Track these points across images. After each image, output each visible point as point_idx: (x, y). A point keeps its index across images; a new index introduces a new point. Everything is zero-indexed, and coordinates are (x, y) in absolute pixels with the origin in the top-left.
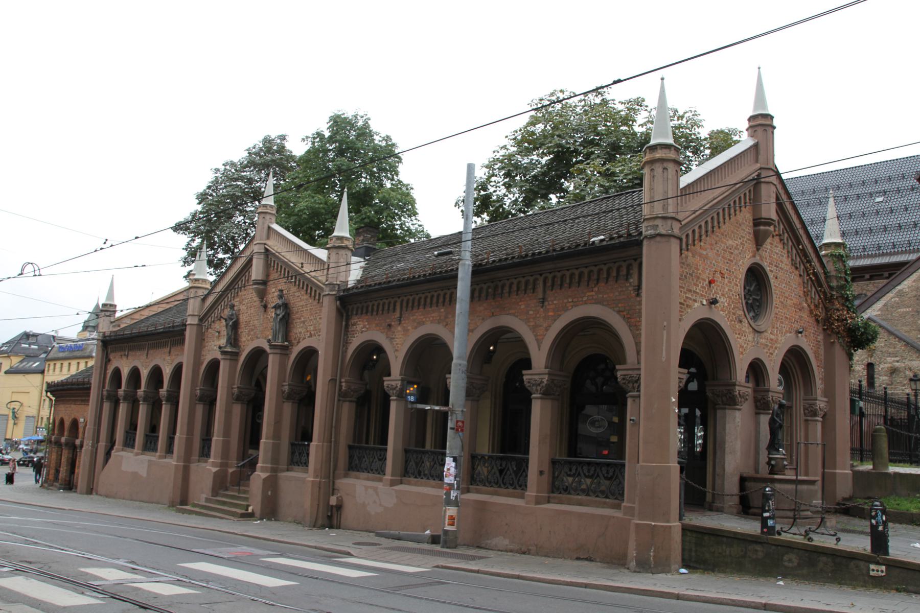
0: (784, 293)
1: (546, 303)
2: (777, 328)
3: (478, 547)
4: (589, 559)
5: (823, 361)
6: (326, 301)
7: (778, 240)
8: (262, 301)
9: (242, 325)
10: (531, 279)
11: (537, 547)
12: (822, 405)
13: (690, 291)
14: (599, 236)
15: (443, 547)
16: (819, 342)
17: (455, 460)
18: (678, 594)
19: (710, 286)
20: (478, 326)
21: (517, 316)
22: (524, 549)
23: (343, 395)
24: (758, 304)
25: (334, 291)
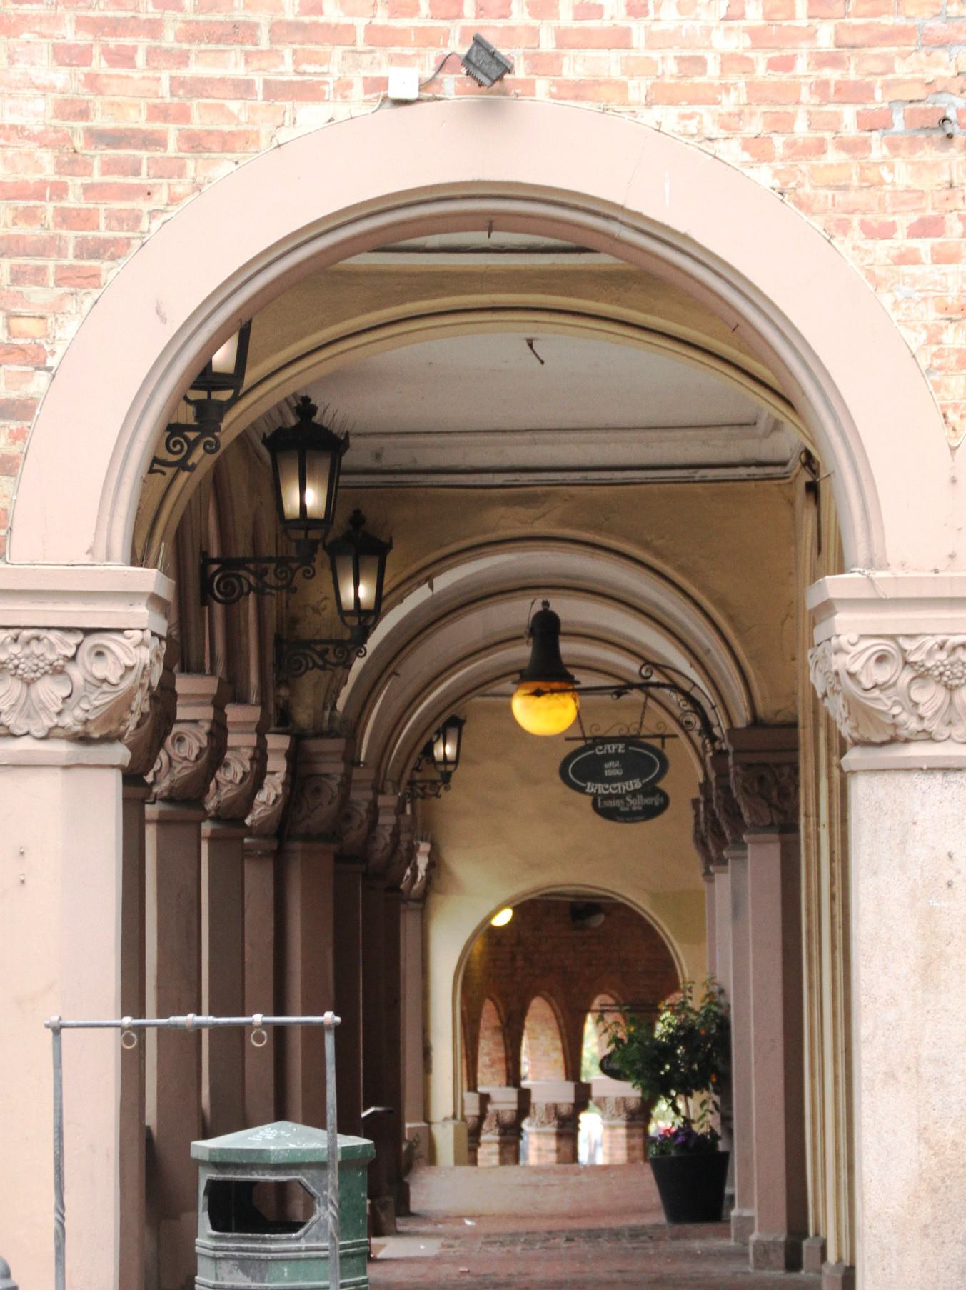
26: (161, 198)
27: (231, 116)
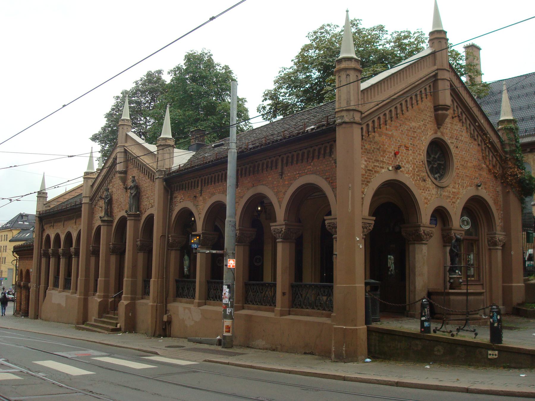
0: (464, 158)
1: (284, 176)
2: (459, 184)
3: (248, 347)
4: (312, 353)
5: (502, 206)
6: (157, 181)
7: (458, 120)
8: (124, 185)
9: (114, 202)
10: (274, 159)
11: (281, 346)
12: (501, 237)
13: (378, 161)
14: (311, 126)
15: (223, 348)
16: (498, 192)
17: (229, 287)
18: (344, 377)
19: (395, 156)
20: (245, 194)
21: (267, 186)
22: (274, 347)
23: (170, 246)
24: (442, 167)
25: (162, 175)
26: (373, 177)
27: (377, 169)
